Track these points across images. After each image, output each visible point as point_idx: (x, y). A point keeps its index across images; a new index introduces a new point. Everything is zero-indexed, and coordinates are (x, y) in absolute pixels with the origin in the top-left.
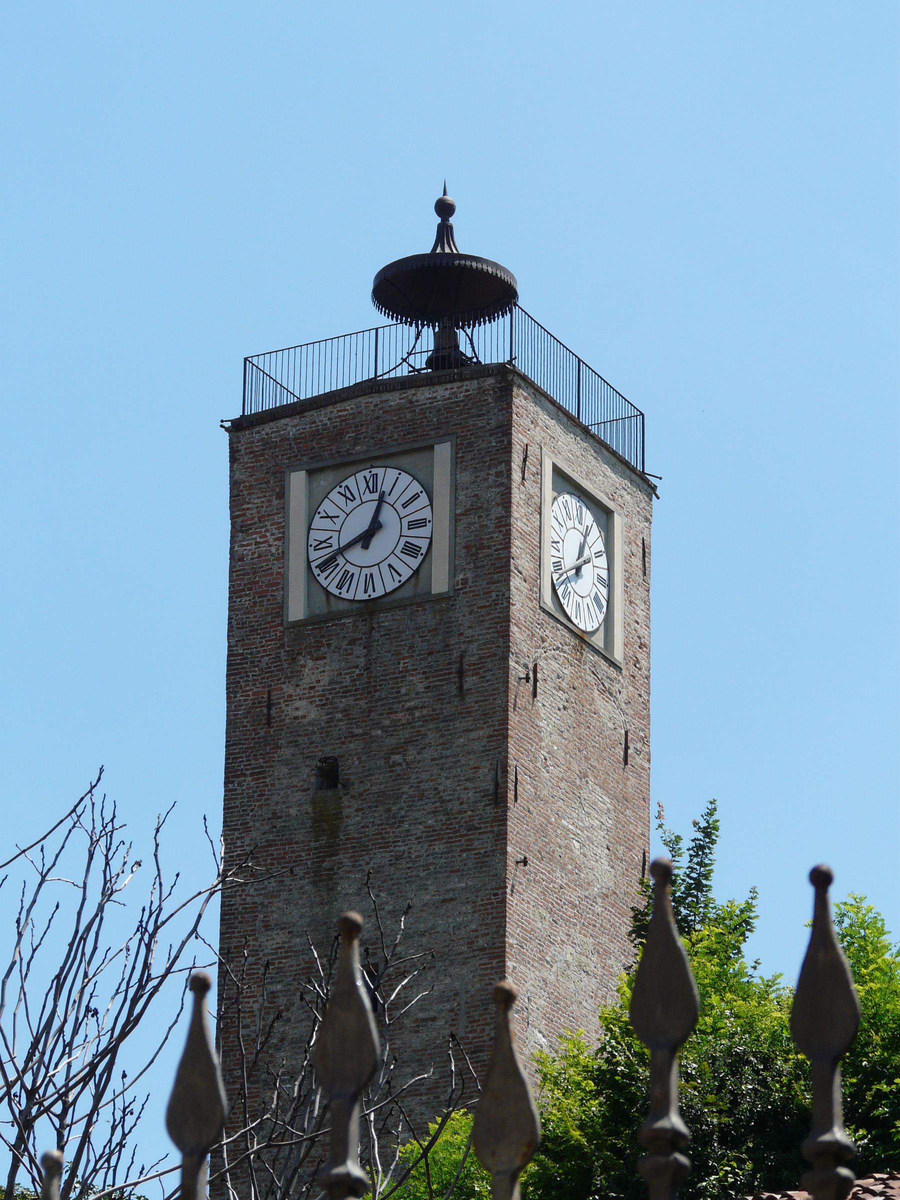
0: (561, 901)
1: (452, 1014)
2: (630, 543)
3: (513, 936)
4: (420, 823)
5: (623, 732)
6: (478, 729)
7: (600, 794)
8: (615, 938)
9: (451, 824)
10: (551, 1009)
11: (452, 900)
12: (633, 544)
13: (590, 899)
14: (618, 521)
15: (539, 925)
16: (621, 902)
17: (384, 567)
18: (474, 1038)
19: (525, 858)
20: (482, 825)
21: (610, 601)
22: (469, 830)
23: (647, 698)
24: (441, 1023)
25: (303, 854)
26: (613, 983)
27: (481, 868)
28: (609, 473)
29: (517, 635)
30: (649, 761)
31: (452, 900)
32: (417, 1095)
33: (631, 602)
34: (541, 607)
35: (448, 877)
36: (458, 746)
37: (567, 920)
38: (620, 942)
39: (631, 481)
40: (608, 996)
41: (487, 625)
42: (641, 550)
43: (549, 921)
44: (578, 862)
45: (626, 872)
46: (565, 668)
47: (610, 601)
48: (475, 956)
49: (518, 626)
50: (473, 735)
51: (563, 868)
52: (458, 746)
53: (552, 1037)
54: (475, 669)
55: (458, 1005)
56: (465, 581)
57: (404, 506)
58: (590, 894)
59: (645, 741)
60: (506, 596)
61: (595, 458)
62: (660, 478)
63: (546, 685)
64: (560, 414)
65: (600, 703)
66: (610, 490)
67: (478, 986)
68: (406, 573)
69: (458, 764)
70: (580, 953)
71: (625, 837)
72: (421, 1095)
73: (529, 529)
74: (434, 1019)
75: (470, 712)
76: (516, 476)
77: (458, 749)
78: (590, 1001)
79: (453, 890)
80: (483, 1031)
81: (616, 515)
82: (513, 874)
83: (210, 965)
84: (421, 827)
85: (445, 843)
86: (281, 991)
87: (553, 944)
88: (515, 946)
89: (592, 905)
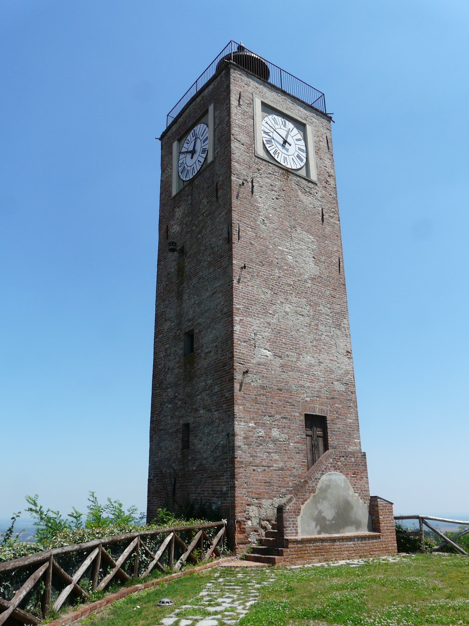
0: (280, 283)
1: (216, 348)
3: (239, 304)
5: (320, 209)
6: (222, 212)
7: (306, 235)
8: (322, 297)
9: (215, 258)
10: (274, 336)
11: (216, 292)
14: (309, 128)
15: (263, 296)
16: (325, 281)
17: (197, 162)
18: (224, 359)
19: (244, 265)
20: (225, 254)
21: (307, 158)
22: (220, 258)
23: (335, 196)
24: (212, 353)
26: (322, 317)
27: (224, 274)
28: (302, 109)
29: (238, 166)
30: (339, 221)
31: (216, 292)
33: (321, 159)
34: (255, 156)
35: (214, 282)
37: (285, 292)
38: (326, 299)
39: (317, 115)
40: (319, 324)
42: (326, 140)
43: (271, 294)
44: (291, 265)
45: (327, 267)
46: (276, 182)
47: (307, 158)
50: (221, 215)
51: (280, 268)
53: (275, 350)
55: (218, 343)
56: (218, 153)
57: (202, 136)
58: (302, 279)
59: (336, 212)
61: (292, 103)
62: (333, 114)
63: (262, 189)
65: (302, 197)
66: (303, 116)
67: (224, 332)
68: (202, 160)
70: (296, 307)
71: (325, 252)
72: (206, 390)
73: (245, 124)
74: (210, 352)
79: (216, 288)
80: (226, 355)
81: (307, 126)
84: (206, 263)
85: (214, 267)
87: (274, 304)
88: (242, 309)
89: (304, 284)
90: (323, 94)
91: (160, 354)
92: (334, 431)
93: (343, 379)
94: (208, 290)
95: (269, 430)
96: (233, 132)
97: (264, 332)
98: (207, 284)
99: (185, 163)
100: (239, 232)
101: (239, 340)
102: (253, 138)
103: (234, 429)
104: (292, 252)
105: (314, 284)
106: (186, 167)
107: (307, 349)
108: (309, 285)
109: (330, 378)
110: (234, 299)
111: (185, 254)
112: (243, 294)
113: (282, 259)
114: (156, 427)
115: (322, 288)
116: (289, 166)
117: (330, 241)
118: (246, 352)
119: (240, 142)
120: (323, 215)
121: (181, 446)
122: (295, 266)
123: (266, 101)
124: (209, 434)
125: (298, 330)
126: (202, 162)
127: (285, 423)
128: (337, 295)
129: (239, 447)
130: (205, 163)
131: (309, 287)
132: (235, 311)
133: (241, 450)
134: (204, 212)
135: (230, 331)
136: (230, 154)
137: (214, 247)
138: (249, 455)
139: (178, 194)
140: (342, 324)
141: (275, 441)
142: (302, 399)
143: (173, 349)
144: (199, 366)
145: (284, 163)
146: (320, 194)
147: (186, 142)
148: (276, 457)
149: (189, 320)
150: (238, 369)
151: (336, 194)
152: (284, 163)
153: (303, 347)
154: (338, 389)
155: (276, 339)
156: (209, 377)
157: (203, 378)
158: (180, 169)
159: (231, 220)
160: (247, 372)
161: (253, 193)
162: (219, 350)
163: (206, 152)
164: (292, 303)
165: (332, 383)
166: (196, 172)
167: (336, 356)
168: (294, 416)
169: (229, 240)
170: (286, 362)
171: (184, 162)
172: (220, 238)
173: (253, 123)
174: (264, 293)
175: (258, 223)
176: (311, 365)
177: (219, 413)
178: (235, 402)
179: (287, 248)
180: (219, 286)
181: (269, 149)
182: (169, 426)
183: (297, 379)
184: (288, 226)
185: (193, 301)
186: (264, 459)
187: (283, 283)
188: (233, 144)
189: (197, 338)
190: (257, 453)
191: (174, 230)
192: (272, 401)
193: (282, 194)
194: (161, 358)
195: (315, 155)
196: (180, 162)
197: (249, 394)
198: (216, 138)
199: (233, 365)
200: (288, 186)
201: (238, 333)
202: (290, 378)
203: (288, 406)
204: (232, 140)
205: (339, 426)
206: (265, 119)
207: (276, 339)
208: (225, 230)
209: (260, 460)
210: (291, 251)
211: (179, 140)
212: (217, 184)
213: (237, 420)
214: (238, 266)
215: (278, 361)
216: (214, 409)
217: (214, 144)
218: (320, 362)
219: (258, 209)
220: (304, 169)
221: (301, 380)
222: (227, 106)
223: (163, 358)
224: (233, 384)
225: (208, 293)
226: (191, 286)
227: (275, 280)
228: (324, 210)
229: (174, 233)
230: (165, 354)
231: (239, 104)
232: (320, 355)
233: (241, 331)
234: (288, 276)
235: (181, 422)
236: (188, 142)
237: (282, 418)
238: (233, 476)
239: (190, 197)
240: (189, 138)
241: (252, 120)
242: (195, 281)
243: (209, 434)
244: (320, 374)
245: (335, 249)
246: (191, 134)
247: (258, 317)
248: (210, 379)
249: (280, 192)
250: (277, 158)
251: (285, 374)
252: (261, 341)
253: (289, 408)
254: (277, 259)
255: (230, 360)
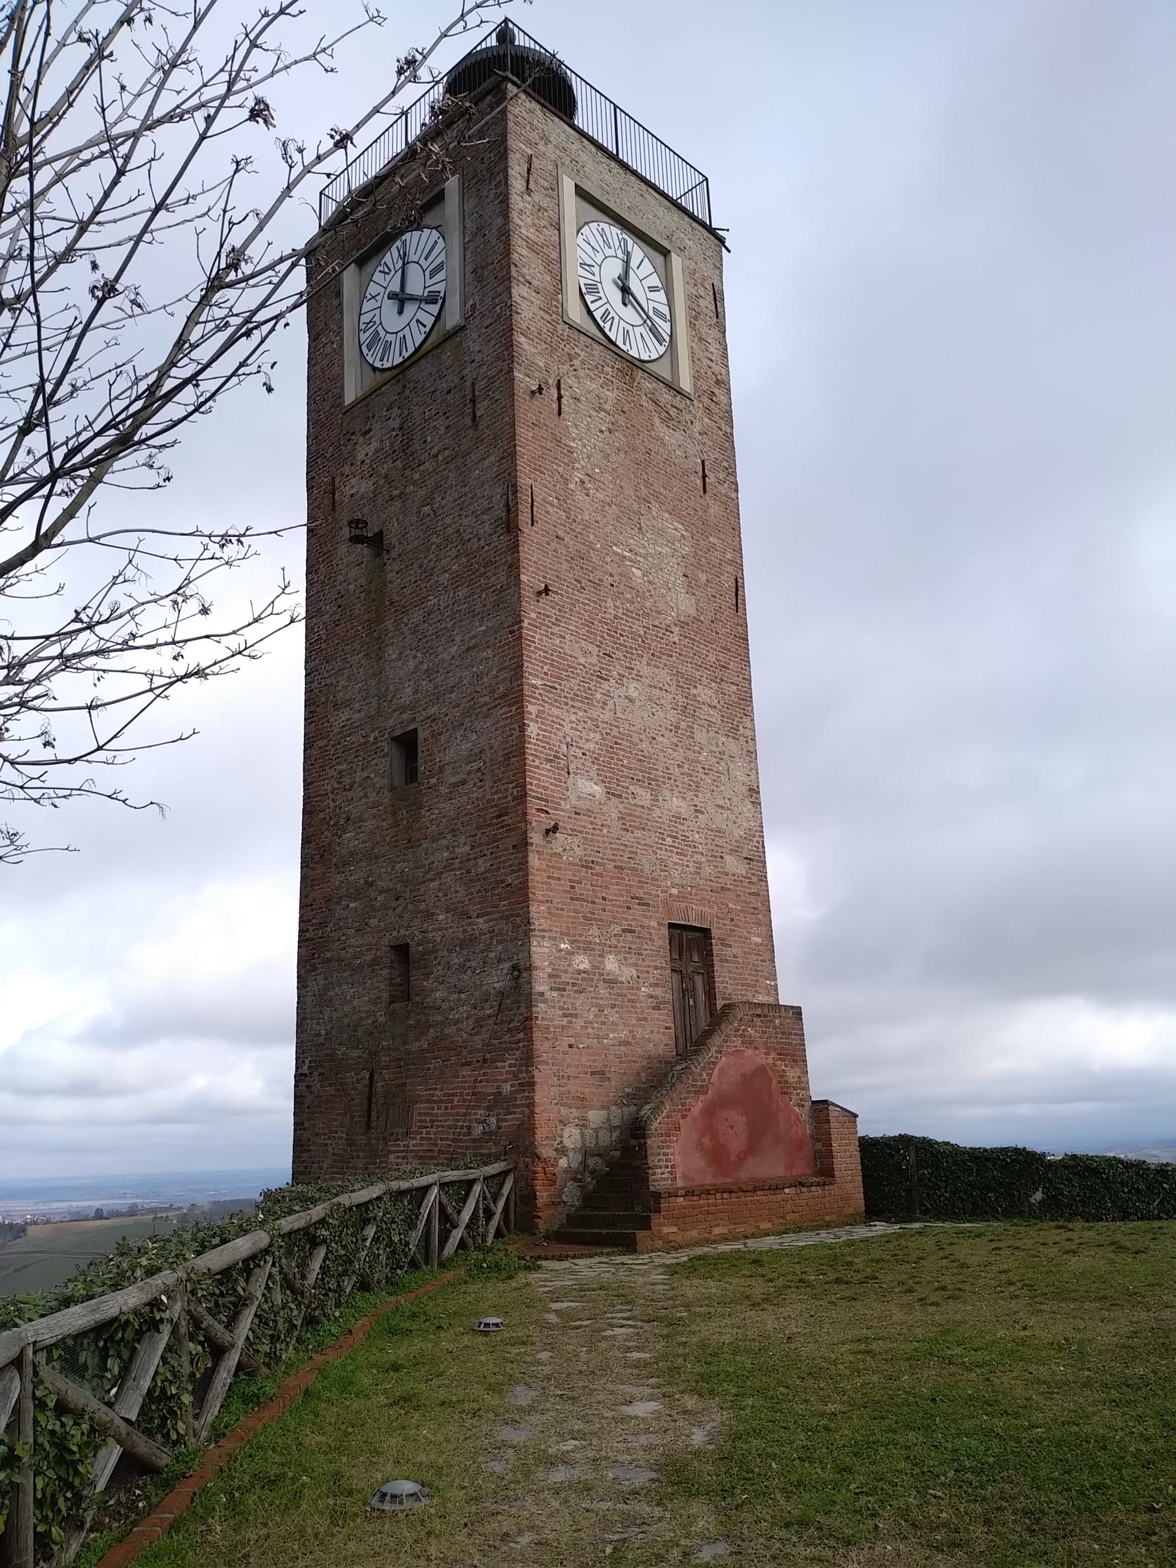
0: (616, 632)
2: (695, 285)
4: (446, 571)
5: (699, 461)
12: (700, 286)
13: (661, 628)
14: (676, 260)
17: (414, 324)
18: (499, 799)
19: (546, 586)
25: (360, 628)
29: (525, 346)
31: (475, 646)
32: (452, 870)
33: (701, 339)
36: (475, 479)
38: (709, 670)
41: (493, 342)
42: (711, 293)
45: (712, 599)
48: (496, 706)
49: (526, 336)
50: (486, 463)
52: (475, 479)
53: (609, 783)
54: (610, 665)
56: (474, 306)
57: (426, 259)
60: (509, 304)
62: (728, 230)
64: (584, 140)
65: (661, 430)
68: (429, 321)
69: (476, 498)
72: (455, 870)
74: (464, 782)
75: (483, 440)
76: (517, 184)
77: (475, 482)
78: (667, 734)
79: (476, 636)
80: (506, 790)
81: (673, 254)
82: (531, 612)
83: (115, 737)
84: (447, 575)
86: (346, 770)
87: (606, 680)
90: (706, 179)
91: (324, 785)
92: (727, 961)
93: (742, 848)
94: (454, 640)
95: (600, 959)
96: (515, 256)
97: (587, 740)
98: (449, 625)
99: (378, 322)
100: (532, 506)
101: (537, 756)
102: (560, 280)
103: (530, 956)
104: (642, 560)
105: (686, 637)
106: (382, 333)
107: (672, 781)
108: (676, 639)
109: (716, 845)
110: (526, 664)
111: (388, 551)
112: (542, 653)
113: (621, 575)
114: (314, 954)
115: (702, 646)
116: (634, 353)
117: (718, 538)
118: (551, 784)
119: (530, 283)
120: (704, 476)
121: (385, 995)
122: (647, 594)
123: (587, 186)
124: (463, 968)
125: (654, 739)
126: (429, 324)
127: (631, 942)
128: (731, 663)
129: (542, 994)
130: (436, 328)
131: (674, 643)
132: (527, 690)
133: (545, 1002)
134: (439, 452)
135: (514, 737)
136: (508, 313)
137: (469, 541)
138: (561, 1013)
139: (363, 401)
140: (741, 728)
141: (611, 982)
142: (662, 891)
143: (359, 776)
144: (433, 814)
145: (625, 344)
146: (697, 427)
147: (380, 268)
148: (613, 1016)
149: (403, 709)
150: (537, 822)
151: (732, 427)
152: (625, 344)
153: (664, 777)
154: (733, 870)
155: (610, 758)
156: (462, 839)
157: (445, 842)
158: (363, 337)
159: (516, 477)
160: (555, 829)
161: (560, 413)
162: (488, 777)
163: (440, 301)
164: (641, 677)
165: (722, 857)
166: (411, 350)
167: (729, 799)
168: (649, 927)
169: (510, 526)
170: (631, 809)
171: (377, 319)
172: (485, 517)
173: (557, 239)
174: (585, 653)
175: (572, 486)
176: (678, 818)
177: (490, 920)
178: (531, 896)
179: (631, 551)
180: (485, 632)
181: (592, 307)
182: (351, 951)
183: (652, 847)
184: (634, 497)
185: (412, 664)
186: (591, 1022)
187: (624, 630)
188: (516, 287)
189: (428, 750)
190: (576, 1009)
191: (354, 491)
192: (604, 895)
193: (622, 420)
194: (327, 794)
195: (689, 329)
196: (365, 318)
197: (560, 879)
198: (469, 268)
199: (525, 814)
200: (633, 401)
201: (535, 741)
202: (639, 843)
203: (637, 906)
204: (514, 278)
205: (735, 950)
206: (582, 231)
207: (610, 758)
208: (498, 500)
209: (583, 1024)
210: (638, 558)
211: (361, 262)
212: (473, 384)
213: (536, 936)
214: (532, 587)
215: (614, 809)
216: (474, 910)
217: (464, 284)
218: (697, 811)
219: (572, 453)
220: (666, 361)
221: (661, 849)
222: (498, 191)
223: (330, 795)
224: (526, 856)
225: (455, 648)
226: (405, 630)
227: (607, 624)
228: (706, 463)
229: (352, 496)
230: (336, 785)
231: (527, 188)
232: (697, 796)
233: (541, 737)
234: (634, 615)
235: (385, 941)
236: (386, 270)
237: (624, 931)
238: (528, 1059)
239: (396, 411)
240: (387, 258)
241: (557, 232)
242: (416, 616)
243: (463, 968)
244: (697, 836)
245: (729, 556)
246: (394, 249)
247: (573, 706)
248: (465, 844)
249: (616, 416)
250: (610, 330)
251: (629, 834)
252: (582, 761)
253: (637, 911)
254: (611, 575)
255: (516, 802)
